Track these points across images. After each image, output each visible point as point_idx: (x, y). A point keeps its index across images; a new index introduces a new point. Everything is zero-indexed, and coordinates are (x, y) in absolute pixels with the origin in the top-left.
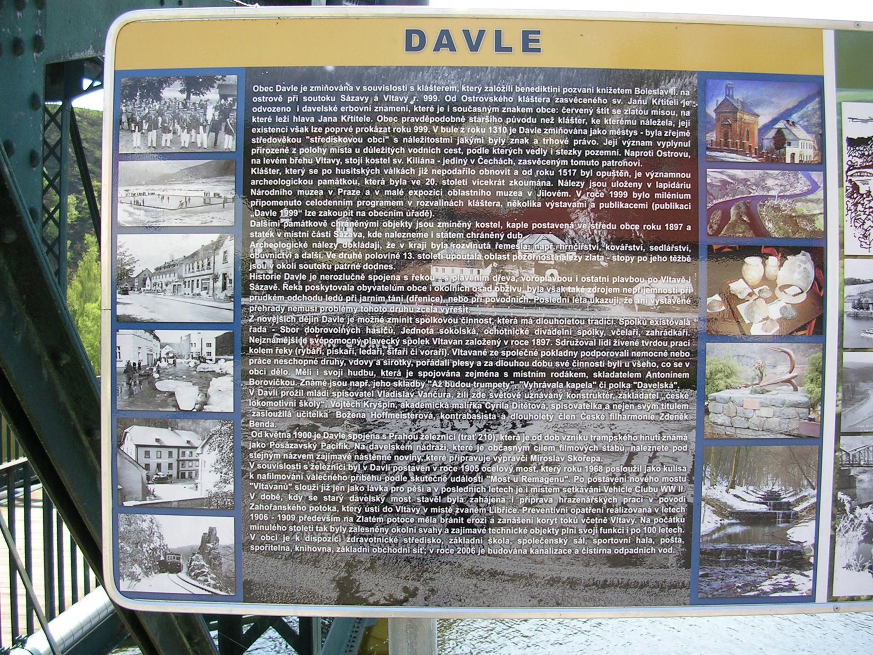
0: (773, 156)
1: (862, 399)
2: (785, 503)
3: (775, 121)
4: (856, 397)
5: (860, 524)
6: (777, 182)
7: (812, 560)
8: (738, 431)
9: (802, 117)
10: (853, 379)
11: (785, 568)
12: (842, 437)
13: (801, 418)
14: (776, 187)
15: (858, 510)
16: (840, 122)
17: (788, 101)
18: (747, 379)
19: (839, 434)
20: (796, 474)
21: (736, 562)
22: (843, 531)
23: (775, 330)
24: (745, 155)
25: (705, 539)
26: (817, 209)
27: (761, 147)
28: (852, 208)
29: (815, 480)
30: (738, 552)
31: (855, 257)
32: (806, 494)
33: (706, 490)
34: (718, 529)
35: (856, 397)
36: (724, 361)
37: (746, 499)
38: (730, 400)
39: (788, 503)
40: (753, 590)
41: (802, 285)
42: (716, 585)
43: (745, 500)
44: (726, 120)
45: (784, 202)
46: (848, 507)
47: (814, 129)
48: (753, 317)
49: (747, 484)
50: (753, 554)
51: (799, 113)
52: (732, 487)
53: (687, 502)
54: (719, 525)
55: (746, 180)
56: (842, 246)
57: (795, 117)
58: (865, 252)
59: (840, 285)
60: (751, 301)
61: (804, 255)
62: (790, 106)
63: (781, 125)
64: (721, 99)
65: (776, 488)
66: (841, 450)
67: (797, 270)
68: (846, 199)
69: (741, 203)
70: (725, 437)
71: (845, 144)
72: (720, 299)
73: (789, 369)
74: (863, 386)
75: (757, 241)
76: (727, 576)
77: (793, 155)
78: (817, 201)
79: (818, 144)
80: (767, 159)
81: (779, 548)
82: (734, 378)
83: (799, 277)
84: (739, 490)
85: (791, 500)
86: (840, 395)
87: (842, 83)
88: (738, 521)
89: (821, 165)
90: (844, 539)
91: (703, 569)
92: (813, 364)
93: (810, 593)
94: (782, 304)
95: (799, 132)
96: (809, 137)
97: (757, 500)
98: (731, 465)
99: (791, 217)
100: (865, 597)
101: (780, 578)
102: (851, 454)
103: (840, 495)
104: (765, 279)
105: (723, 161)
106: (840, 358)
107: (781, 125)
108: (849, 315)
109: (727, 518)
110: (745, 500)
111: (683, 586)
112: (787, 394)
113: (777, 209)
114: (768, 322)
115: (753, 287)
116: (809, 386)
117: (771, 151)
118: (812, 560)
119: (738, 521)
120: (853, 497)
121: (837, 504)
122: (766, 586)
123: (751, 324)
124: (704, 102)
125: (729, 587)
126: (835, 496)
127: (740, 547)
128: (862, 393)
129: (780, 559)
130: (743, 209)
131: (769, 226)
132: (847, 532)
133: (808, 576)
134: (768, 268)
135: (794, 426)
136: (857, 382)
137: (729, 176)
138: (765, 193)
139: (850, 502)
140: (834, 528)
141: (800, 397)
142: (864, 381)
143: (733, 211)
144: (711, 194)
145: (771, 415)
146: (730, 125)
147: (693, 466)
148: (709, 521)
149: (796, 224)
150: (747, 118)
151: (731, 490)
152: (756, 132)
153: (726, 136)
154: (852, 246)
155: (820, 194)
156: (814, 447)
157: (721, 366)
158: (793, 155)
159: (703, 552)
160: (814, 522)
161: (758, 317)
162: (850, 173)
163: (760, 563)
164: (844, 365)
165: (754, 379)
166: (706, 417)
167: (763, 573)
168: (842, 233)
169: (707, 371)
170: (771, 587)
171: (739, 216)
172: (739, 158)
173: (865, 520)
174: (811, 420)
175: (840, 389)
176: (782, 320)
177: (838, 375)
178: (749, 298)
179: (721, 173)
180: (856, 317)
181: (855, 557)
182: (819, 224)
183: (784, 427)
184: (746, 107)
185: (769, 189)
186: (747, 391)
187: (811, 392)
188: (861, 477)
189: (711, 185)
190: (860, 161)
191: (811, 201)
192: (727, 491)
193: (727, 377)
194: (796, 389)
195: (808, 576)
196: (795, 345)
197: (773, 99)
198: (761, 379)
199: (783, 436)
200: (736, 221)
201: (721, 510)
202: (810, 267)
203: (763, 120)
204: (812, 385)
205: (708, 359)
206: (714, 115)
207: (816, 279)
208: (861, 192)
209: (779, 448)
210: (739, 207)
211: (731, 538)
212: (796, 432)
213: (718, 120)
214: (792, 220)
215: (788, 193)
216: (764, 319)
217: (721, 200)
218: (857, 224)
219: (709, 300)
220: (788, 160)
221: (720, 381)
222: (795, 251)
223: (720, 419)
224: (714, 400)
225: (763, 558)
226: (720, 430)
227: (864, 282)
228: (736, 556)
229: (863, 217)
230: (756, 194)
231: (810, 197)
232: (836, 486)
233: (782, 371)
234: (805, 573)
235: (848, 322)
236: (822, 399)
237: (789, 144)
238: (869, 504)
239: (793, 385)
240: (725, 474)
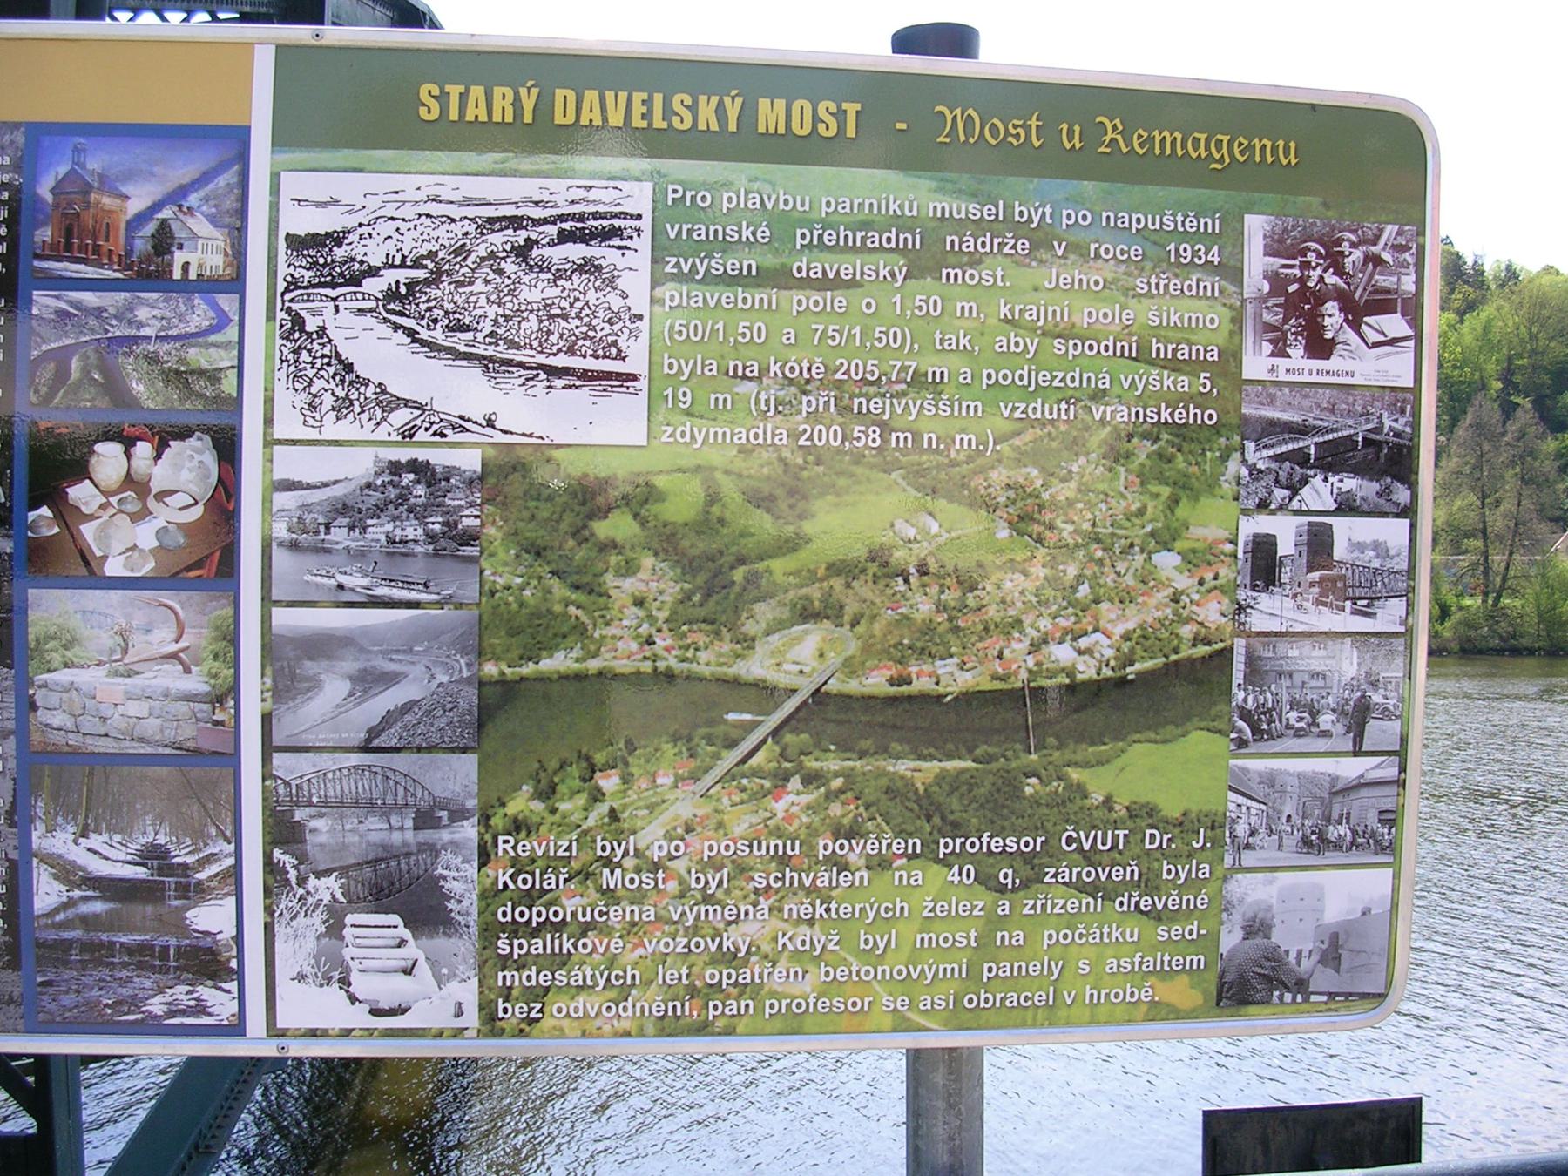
0: (151, 269)
1: (309, 690)
2: (179, 865)
3: (157, 206)
4: (298, 686)
5: (317, 906)
6: (155, 312)
7: (234, 964)
8: (89, 740)
9: (206, 199)
10: (292, 654)
11: (185, 975)
12: (275, 755)
13: (198, 720)
14: (153, 321)
15: (312, 882)
16: (275, 207)
17: (182, 170)
18: (100, 652)
19: (269, 749)
20: (195, 815)
21: (99, 963)
22: (287, 916)
23: (147, 568)
24: (101, 266)
25: (43, 921)
26: (226, 359)
27: (129, 253)
28: (291, 356)
29: (230, 827)
30: (102, 945)
31: (295, 442)
32: (215, 851)
33: (38, 839)
34: (65, 906)
35: (298, 686)
36: (60, 621)
37: (110, 856)
38: (71, 687)
39: (185, 866)
40: (133, 1012)
41: (195, 490)
42: (67, 1000)
43: (107, 858)
44: (70, 205)
45: (166, 346)
46: (292, 875)
47: (227, 220)
48: (108, 546)
49: (108, 830)
50: (129, 950)
51: (202, 193)
52: (84, 835)
53: (7, 859)
54: (65, 899)
55: (101, 310)
56: (269, 421)
57: (193, 199)
58: (313, 434)
59: (264, 490)
60: (105, 518)
61: (199, 439)
62: (186, 180)
63: (166, 213)
64: (63, 170)
65: (161, 840)
66: (276, 778)
67: (187, 464)
68: (279, 342)
69: (90, 350)
70: (66, 749)
71: (282, 245)
72: (50, 514)
73: (173, 636)
74: (310, 668)
75: (114, 418)
76: (85, 985)
77: (186, 267)
78: (226, 346)
79: (233, 246)
80: (139, 274)
81: (173, 942)
82: (76, 649)
83: (191, 476)
84: (95, 841)
85: (190, 859)
86: (269, 681)
87: (280, 140)
88: (97, 894)
89: (235, 282)
90: (289, 930)
91: (43, 973)
92: (217, 628)
93: (235, 1020)
94: (161, 522)
95: (200, 225)
96: (216, 233)
97: (129, 858)
98: (80, 797)
99: (177, 372)
100: (337, 1031)
101: (180, 993)
102: (294, 784)
103: (277, 854)
104: (129, 481)
105: (62, 278)
106: (266, 619)
107: (166, 213)
108: (280, 544)
109: (79, 887)
110: (107, 858)
111: (11, 1001)
112: (171, 679)
113: (153, 359)
114: (136, 554)
115: (106, 494)
116: (210, 664)
117: (149, 260)
118: (234, 964)
119: (97, 894)
120: (302, 858)
121: (270, 866)
122: (156, 1006)
123: (105, 557)
124: (34, 180)
125: (91, 1005)
126: (268, 857)
127: (104, 937)
128: (308, 679)
129: (176, 961)
130: (93, 359)
131: (138, 388)
132: (294, 918)
133: (228, 992)
134: (134, 462)
135: (186, 733)
136: (299, 659)
137: (71, 303)
138: (134, 332)
139: (296, 867)
140: (269, 911)
141: (196, 683)
142: (311, 659)
143: (75, 364)
144: (39, 335)
145: (145, 713)
146: (78, 214)
147: (14, 796)
148: (47, 893)
149: (187, 385)
150: (107, 201)
151: (81, 840)
152: (123, 226)
153: (69, 234)
154: (288, 424)
155: (232, 333)
156: (224, 771)
157: (54, 628)
158: (186, 267)
159: (40, 944)
160: (233, 899)
161: (117, 546)
162: (288, 296)
163: (141, 966)
164: (274, 630)
165: (112, 652)
166: (32, 716)
167: (148, 984)
168: (269, 401)
169: (31, 637)
170: (165, 1008)
171: (86, 371)
172: (88, 271)
173: (327, 898)
174: (216, 723)
175: (269, 671)
176: (160, 551)
177: (263, 647)
178: (101, 512)
179: (57, 297)
180: (294, 546)
181: (313, 962)
182: (229, 385)
183: (170, 735)
184: (107, 183)
185: (141, 325)
186: (101, 672)
187: (215, 676)
188: (313, 824)
189: (39, 318)
190: (308, 275)
191: (215, 345)
192: (75, 842)
193: (65, 647)
194: (187, 671)
195: (228, 992)
196: (184, 595)
197: (155, 169)
198: (125, 651)
199: (168, 751)
200: (80, 380)
201: (66, 872)
202: (210, 459)
203: (135, 206)
204: (216, 664)
205: (32, 616)
206: (49, 198)
207: (220, 479)
208: (308, 329)
209: (162, 771)
210: (85, 357)
211: (86, 921)
212: (190, 744)
213: (56, 206)
214: (180, 378)
215: (174, 332)
216: (128, 550)
217: (53, 345)
218: (297, 385)
219: (32, 516)
220: (177, 275)
221: (54, 654)
222: (183, 434)
223: (57, 719)
224: (45, 686)
225: (144, 957)
226: (57, 738)
227: (309, 487)
228: (97, 953)
229: (311, 373)
230: (118, 333)
231: (212, 338)
232: (268, 838)
233: (163, 639)
234: (224, 986)
235: (278, 555)
236: (235, 689)
237: (181, 247)
238: (334, 870)
239: (182, 662)
240: (71, 813)
